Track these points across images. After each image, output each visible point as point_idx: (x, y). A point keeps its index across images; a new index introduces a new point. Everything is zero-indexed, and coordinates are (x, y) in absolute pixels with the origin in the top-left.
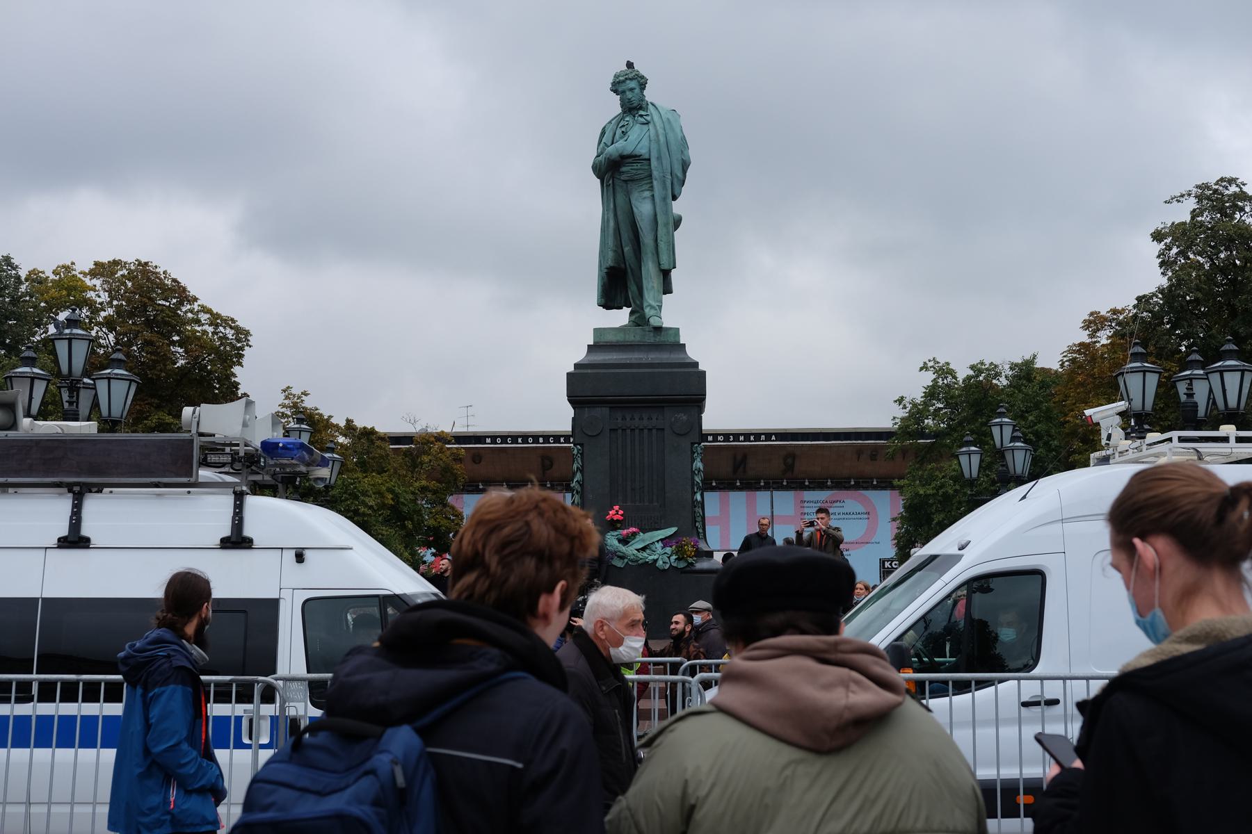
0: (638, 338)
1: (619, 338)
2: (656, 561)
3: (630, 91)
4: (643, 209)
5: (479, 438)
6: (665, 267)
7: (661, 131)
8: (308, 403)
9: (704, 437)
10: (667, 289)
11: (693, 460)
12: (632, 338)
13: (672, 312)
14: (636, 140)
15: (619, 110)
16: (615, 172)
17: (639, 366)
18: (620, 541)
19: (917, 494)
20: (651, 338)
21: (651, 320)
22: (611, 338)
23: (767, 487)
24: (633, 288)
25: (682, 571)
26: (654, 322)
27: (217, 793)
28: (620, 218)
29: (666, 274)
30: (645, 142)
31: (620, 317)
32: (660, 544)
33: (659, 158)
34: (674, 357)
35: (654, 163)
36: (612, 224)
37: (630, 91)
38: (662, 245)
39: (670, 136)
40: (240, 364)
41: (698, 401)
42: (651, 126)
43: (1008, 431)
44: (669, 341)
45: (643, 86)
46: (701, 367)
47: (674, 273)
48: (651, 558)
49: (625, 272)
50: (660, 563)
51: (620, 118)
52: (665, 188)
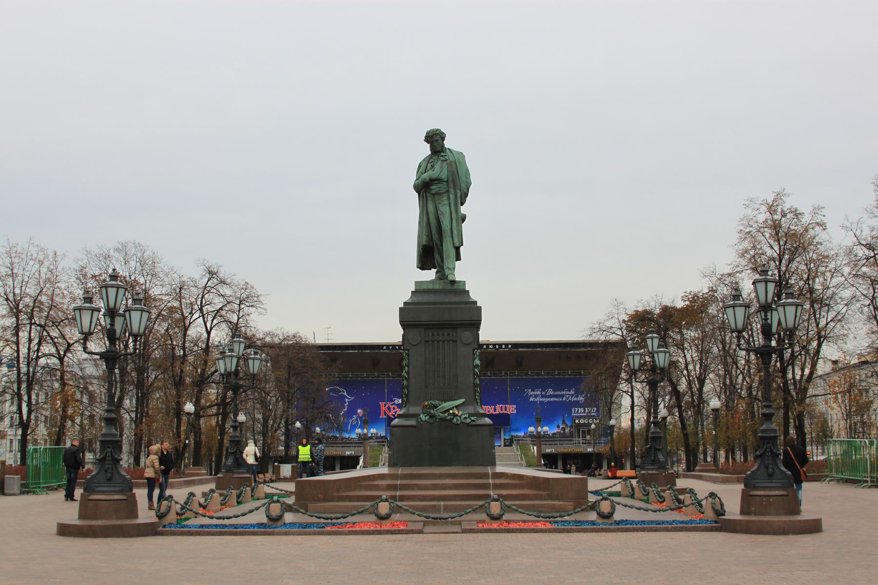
0: (441, 287)
1: (431, 287)
3: (435, 139)
6: (457, 245)
9: (480, 346)
10: (458, 258)
11: (474, 359)
13: (461, 272)
15: (430, 153)
17: (442, 303)
20: (448, 287)
22: (425, 287)
24: (437, 256)
25: (468, 425)
26: (450, 278)
27: (301, 477)
29: (457, 249)
30: (445, 171)
31: (430, 275)
34: (465, 299)
37: (435, 139)
38: (455, 232)
41: (476, 324)
43: (656, 341)
44: (458, 290)
45: (443, 139)
46: (478, 304)
47: (462, 248)
51: (430, 157)
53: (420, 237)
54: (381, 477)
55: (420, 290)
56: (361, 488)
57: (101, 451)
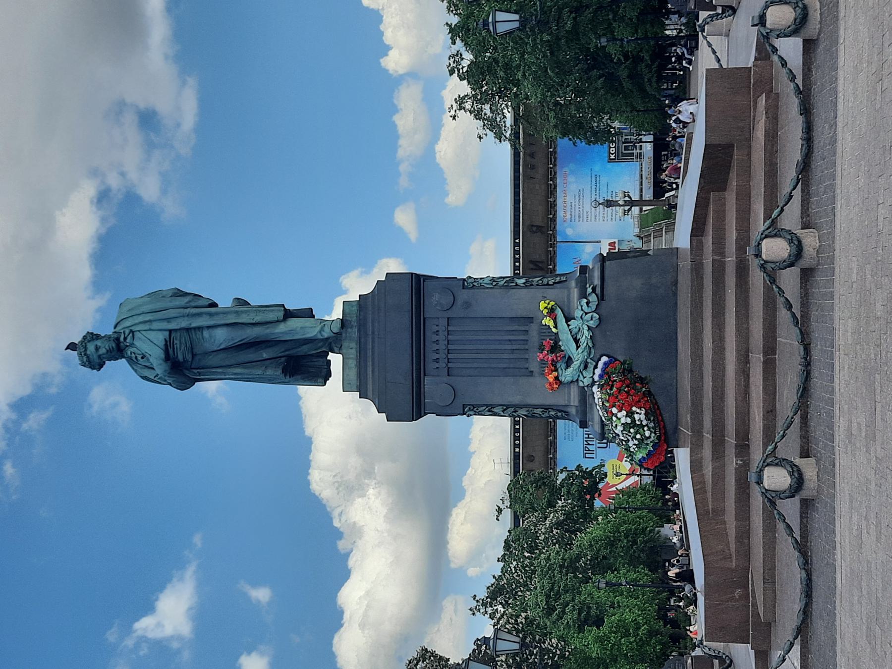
0: (353, 345)
1: (352, 363)
2: (589, 328)
4: (221, 337)
5: (516, 457)
6: (281, 315)
7: (141, 318)
8: (482, 594)
10: (308, 313)
12: (354, 351)
14: (150, 344)
15: (123, 361)
16: (183, 366)
18: (568, 366)
19: (555, 126)
20: (354, 332)
21: (335, 330)
22: (353, 374)
23: (553, 246)
24: (304, 350)
25: (601, 298)
26: (336, 328)
28: (233, 362)
29: (289, 315)
30: (152, 335)
32: (571, 322)
33: (168, 320)
35: (173, 326)
36: (238, 370)
39: (145, 308)
40: (448, 660)
42: (133, 328)
45: (97, 337)
48: (586, 332)
49: (290, 358)
50: (592, 324)
51: (132, 362)
52: (200, 315)
53: (271, 381)
54: (696, 466)
55: (360, 384)
56: (719, 512)
57: (640, 408)
